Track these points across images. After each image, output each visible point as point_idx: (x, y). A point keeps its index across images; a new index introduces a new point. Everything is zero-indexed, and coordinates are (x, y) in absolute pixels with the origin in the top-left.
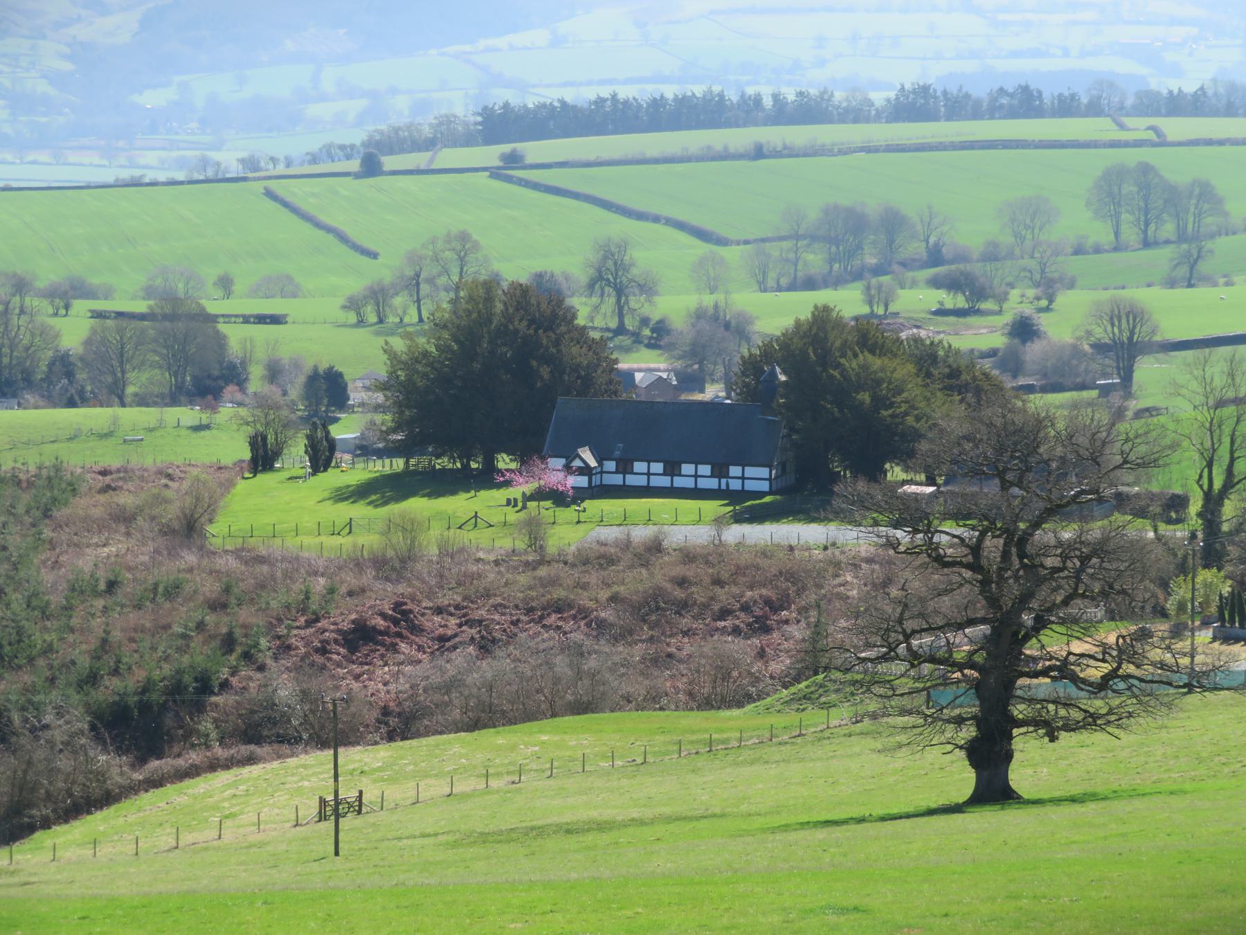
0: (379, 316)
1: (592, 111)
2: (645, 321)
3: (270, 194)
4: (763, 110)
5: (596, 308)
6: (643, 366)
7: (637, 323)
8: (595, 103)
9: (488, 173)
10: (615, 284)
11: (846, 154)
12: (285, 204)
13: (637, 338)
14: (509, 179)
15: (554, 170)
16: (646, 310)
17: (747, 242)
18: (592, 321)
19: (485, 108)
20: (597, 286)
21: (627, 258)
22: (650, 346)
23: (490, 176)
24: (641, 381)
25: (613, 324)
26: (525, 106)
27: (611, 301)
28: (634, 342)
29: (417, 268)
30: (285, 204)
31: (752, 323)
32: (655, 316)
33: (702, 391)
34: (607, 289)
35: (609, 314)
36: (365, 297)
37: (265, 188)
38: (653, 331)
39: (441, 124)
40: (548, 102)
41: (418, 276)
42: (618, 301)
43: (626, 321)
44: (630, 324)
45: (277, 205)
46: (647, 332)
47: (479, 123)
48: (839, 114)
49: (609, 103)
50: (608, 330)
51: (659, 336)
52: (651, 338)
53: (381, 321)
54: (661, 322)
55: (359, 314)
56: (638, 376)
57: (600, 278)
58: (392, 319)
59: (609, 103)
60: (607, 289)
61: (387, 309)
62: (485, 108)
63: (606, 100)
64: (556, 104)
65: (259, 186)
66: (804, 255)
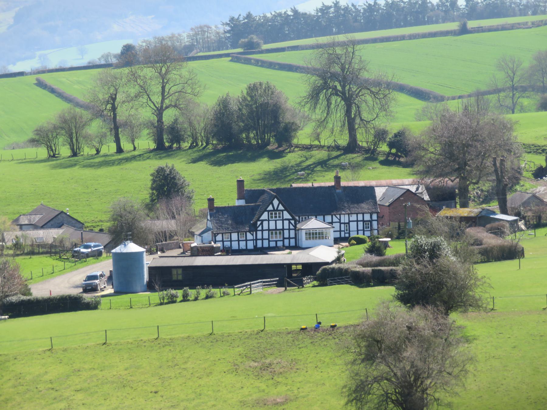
0: (72, 149)
1: (319, 17)
2: (381, 135)
3: (41, 84)
4: (459, 9)
5: (322, 123)
6: (384, 182)
7: (371, 138)
8: (321, 10)
9: (230, 58)
10: (343, 93)
11: (539, 26)
12: (53, 91)
13: (371, 155)
14: (248, 62)
15: (287, 53)
16: (382, 123)
17: (460, 97)
18: (318, 138)
19: (232, 19)
20: (322, 96)
21: (356, 60)
22: (386, 163)
23: (231, 61)
24: (383, 198)
25: (344, 141)
26: (265, 17)
27: (338, 115)
28: (366, 159)
29: (112, 90)
30: (53, 91)
31: (511, 129)
32: (393, 127)
33: (372, 270)
34: (334, 99)
35: (337, 129)
36: (55, 128)
37: (37, 79)
38: (391, 145)
39: (196, 34)
40: (283, 11)
41: (114, 99)
42: (348, 112)
43: (359, 137)
44: (363, 139)
45: (45, 92)
46: (384, 148)
47: (228, 32)
48: (520, 10)
49: (332, 10)
50: (337, 148)
51: (400, 151)
52: (389, 154)
53: (75, 154)
54: (400, 134)
55: (50, 148)
56: (379, 192)
57: (325, 86)
58: (87, 150)
59: (332, 10)
60: (334, 99)
61: (81, 139)
62: (232, 19)
63: (331, 7)
64: (290, 13)
65: (32, 79)
66: (520, 100)
